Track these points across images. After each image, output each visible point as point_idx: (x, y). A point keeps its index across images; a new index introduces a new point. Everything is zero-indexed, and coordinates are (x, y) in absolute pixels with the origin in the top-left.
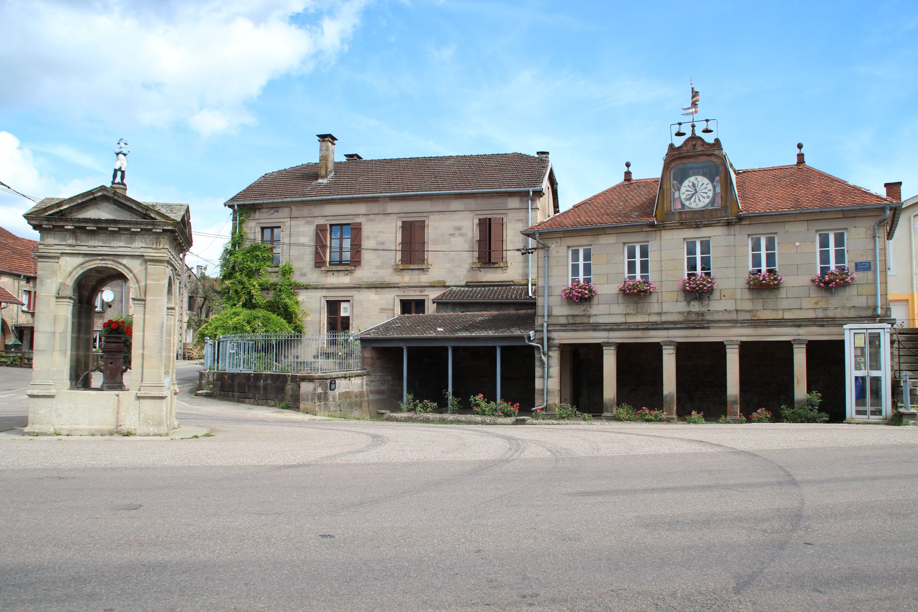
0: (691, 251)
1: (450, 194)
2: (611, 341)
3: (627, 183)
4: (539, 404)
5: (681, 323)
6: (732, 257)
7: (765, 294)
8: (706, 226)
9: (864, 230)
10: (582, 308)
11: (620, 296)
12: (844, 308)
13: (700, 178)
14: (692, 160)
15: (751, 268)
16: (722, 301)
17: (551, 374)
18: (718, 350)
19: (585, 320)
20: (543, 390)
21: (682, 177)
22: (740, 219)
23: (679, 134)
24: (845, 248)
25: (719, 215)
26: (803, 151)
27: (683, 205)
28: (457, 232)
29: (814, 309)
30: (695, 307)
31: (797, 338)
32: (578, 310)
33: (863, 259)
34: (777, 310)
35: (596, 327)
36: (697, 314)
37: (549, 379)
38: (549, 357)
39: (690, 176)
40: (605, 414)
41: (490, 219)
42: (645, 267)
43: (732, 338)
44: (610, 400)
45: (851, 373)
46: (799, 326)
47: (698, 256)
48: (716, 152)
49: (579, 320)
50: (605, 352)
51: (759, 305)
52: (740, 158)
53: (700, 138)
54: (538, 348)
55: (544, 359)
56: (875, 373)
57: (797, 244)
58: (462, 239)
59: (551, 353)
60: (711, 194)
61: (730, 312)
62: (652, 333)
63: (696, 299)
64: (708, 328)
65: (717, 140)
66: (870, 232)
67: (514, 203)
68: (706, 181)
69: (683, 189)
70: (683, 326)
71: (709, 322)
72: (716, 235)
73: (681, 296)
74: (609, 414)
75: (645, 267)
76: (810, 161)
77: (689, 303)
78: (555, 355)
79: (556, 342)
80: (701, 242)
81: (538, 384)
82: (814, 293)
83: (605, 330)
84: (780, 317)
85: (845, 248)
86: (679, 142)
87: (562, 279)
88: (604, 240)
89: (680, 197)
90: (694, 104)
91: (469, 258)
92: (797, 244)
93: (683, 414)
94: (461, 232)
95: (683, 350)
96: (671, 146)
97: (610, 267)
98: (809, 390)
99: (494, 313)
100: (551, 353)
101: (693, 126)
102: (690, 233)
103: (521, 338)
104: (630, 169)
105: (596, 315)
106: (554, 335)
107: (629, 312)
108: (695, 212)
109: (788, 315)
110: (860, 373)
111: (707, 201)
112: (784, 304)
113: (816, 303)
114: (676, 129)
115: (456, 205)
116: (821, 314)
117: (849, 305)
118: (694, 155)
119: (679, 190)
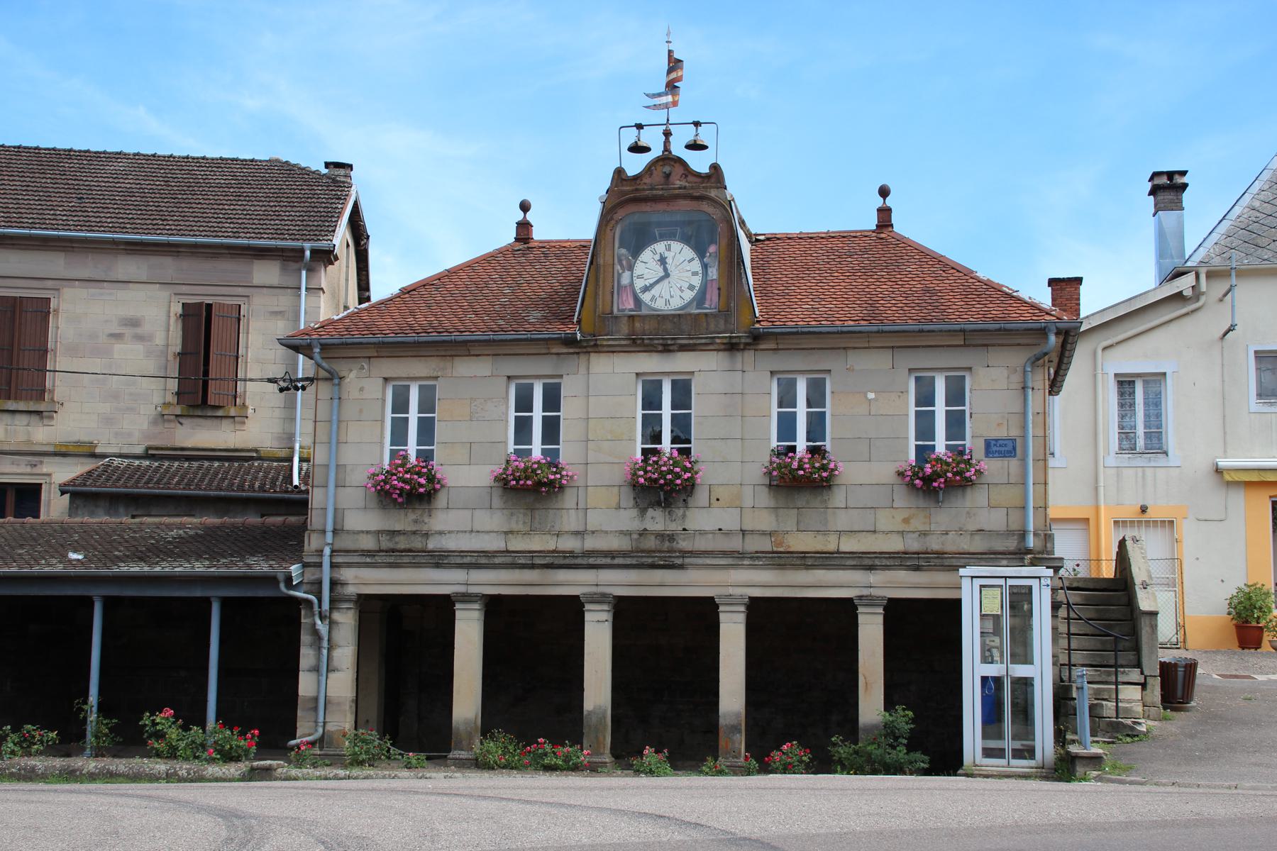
1: (222, 246)
2: (473, 590)
3: (520, 246)
4: (306, 730)
5: (624, 554)
6: (737, 417)
7: (802, 499)
8: (684, 348)
9: (1005, 373)
11: (497, 493)
12: (961, 531)
13: (676, 246)
14: (661, 206)
15: (774, 443)
18: (703, 614)
19: (417, 543)
20: (316, 699)
21: (639, 241)
23: (637, 149)
25: (712, 327)
28: (128, 331)
29: (902, 533)
30: (657, 521)
31: (865, 592)
32: (402, 521)
33: (1001, 433)
34: (826, 532)
35: (440, 560)
36: (660, 536)
37: (331, 677)
40: (455, 754)
41: (209, 306)
42: (551, 430)
43: (731, 591)
46: (871, 568)
48: (713, 193)
49: (402, 543)
51: (789, 520)
52: (766, 204)
53: (680, 161)
54: (309, 602)
56: (1021, 671)
57: (871, 396)
58: (139, 347)
59: (337, 616)
60: (697, 281)
62: (562, 575)
63: (659, 504)
65: (715, 168)
66: (1016, 378)
67: (266, 272)
68: (688, 252)
69: (639, 268)
70: (628, 561)
71: (685, 554)
72: (706, 370)
73: (627, 497)
74: (464, 755)
75: (551, 430)
77: (643, 511)
78: (347, 620)
79: (351, 590)
80: (674, 383)
81: (306, 685)
82: (902, 499)
84: (832, 547)
86: (635, 165)
87: (369, 449)
89: (632, 284)
91: (158, 392)
92: (871, 396)
93: (626, 754)
94: (139, 331)
95: (628, 613)
96: (619, 172)
97: (476, 427)
98: (889, 705)
100: (337, 616)
101: (667, 134)
102: (651, 363)
103: (271, 580)
105: (441, 533)
106: (347, 574)
107: (515, 527)
108: (662, 318)
109: (848, 545)
110: (992, 670)
111: (689, 295)
112: (842, 521)
113: (906, 521)
114: (630, 137)
115: (128, 267)
116: (914, 545)
117: (972, 527)
118: (666, 195)
119: (631, 268)
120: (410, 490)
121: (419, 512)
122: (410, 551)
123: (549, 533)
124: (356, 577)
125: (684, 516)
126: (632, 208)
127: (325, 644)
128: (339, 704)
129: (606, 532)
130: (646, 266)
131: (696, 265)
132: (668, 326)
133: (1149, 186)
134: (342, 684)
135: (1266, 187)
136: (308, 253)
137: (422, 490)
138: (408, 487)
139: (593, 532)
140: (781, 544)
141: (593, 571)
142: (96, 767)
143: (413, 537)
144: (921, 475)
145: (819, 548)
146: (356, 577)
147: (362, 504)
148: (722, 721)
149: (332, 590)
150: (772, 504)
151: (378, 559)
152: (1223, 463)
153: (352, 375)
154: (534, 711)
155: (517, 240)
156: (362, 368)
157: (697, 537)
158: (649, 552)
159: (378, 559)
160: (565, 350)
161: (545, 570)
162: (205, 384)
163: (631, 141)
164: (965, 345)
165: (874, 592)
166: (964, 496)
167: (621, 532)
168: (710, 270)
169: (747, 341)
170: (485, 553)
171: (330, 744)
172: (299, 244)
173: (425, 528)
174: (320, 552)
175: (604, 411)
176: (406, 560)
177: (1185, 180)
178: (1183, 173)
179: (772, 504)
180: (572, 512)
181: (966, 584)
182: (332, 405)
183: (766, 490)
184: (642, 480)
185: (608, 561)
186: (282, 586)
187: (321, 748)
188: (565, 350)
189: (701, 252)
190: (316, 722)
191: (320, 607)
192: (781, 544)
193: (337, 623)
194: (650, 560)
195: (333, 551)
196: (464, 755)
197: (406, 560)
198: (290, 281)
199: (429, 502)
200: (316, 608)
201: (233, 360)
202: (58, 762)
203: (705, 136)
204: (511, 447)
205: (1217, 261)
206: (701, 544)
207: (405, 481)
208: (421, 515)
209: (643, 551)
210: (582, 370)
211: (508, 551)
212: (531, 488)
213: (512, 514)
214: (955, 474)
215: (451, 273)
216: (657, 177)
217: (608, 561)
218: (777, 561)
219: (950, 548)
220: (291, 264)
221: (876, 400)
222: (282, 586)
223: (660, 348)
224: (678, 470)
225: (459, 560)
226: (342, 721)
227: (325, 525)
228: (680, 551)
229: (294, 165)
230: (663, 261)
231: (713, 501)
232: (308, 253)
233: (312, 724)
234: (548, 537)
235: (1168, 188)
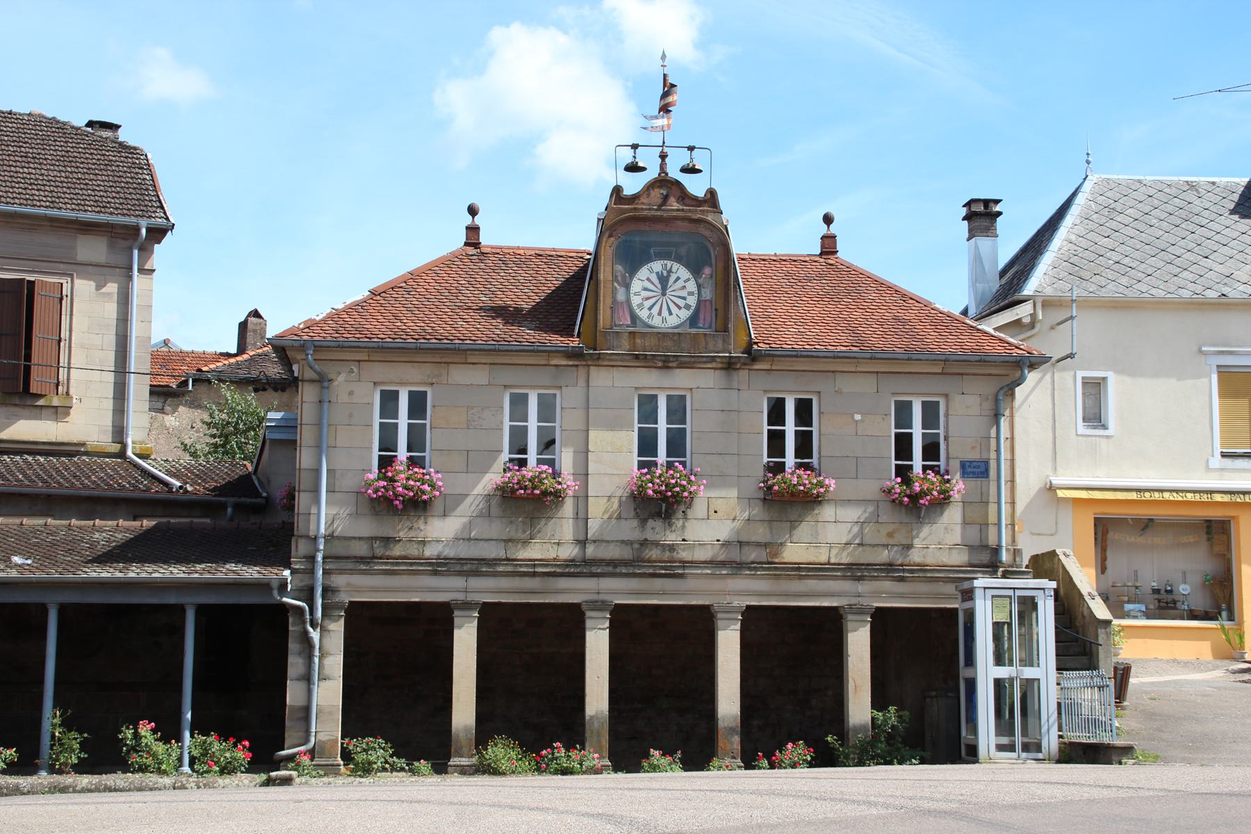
2: (472, 597)
3: (471, 251)
5: (626, 563)
8: (683, 365)
9: (978, 400)
14: (659, 227)
15: (766, 459)
16: (713, 522)
17: (327, 671)
18: (700, 623)
19: (413, 551)
21: (633, 259)
22: (752, 355)
23: (633, 168)
24: (428, 422)
25: (711, 346)
26: (834, 229)
27: (634, 318)
29: (886, 546)
31: (854, 601)
38: (323, 630)
39: (650, 260)
40: (454, 761)
44: (467, 729)
45: (987, 672)
47: (662, 426)
48: (710, 218)
53: (678, 183)
55: (315, 635)
56: (1029, 673)
57: (858, 417)
60: (692, 301)
62: (563, 583)
64: (681, 576)
65: (712, 194)
66: (988, 405)
67: (92, 249)
69: (636, 285)
71: (685, 564)
72: (698, 385)
74: (464, 761)
77: (643, 522)
78: (337, 628)
79: (345, 598)
80: (669, 398)
81: (294, 694)
83: (460, 573)
85: (428, 422)
86: (633, 184)
88: (461, 375)
89: (628, 301)
90: (665, 109)
92: (858, 417)
93: (627, 756)
95: (625, 623)
96: (617, 190)
98: (879, 702)
99: (147, 523)
101: (663, 156)
102: (648, 379)
104: (478, 220)
106: (339, 581)
107: (513, 535)
108: (663, 336)
110: (1003, 672)
111: (685, 314)
113: (890, 535)
114: (627, 156)
118: (662, 218)
119: (627, 287)
125: (683, 527)
127: (317, 653)
128: (330, 713)
129: (608, 542)
130: (644, 280)
133: (964, 211)
135: (1078, 222)
137: (425, 497)
139: (595, 541)
141: (595, 579)
142: (90, 783)
148: (721, 724)
152: (1056, 481)
153: (341, 378)
154: (533, 716)
155: (466, 244)
156: (352, 371)
157: (697, 549)
160: (564, 362)
161: (546, 578)
162: (28, 370)
163: (629, 160)
164: (942, 374)
166: (942, 513)
167: (623, 542)
168: (703, 291)
170: (482, 561)
172: (133, 220)
177: (998, 208)
178: (997, 202)
181: (978, 594)
184: (650, 492)
186: (275, 593)
188: (564, 362)
189: (696, 271)
196: (464, 761)
198: (120, 259)
201: (55, 343)
202: (95, 779)
203: (700, 160)
205: (1049, 291)
207: (406, 488)
214: (939, 493)
215: (414, 276)
216: (657, 194)
217: (610, 569)
220: (120, 241)
221: (862, 421)
222: (275, 593)
224: (684, 483)
225: (458, 568)
229: (64, 124)
232: (144, 231)
233: (301, 734)
235: (982, 216)
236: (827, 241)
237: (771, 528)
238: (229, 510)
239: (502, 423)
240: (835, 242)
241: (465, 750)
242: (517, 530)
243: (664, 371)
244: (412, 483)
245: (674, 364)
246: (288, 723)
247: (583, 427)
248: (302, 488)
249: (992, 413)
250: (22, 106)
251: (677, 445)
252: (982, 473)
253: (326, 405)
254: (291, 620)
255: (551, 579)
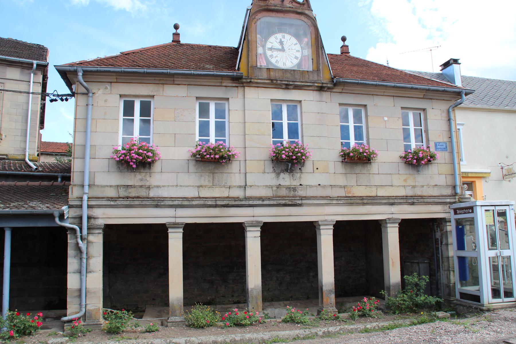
0: (277, 114)
2: (179, 220)
4: (73, 310)
5: (269, 199)
6: (322, 125)
7: (358, 169)
10: (139, 176)
11: (192, 164)
12: (428, 186)
13: (287, 36)
17: (91, 267)
19: (143, 193)
20: (80, 290)
29: (404, 186)
30: (286, 180)
31: (390, 216)
32: (133, 179)
34: (370, 186)
35: (158, 203)
36: (289, 188)
37: (86, 276)
40: (172, 319)
42: (220, 128)
43: (326, 218)
46: (392, 204)
48: (307, 12)
49: (133, 193)
50: (170, 235)
51: (352, 180)
54: (73, 230)
57: (386, 119)
59: (91, 238)
60: (299, 55)
61: (324, 187)
63: (287, 170)
64: (300, 205)
66: (445, 115)
68: (294, 40)
70: (272, 202)
71: (302, 198)
72: (308, 99)
73: (269, 167)
74: (178, 319)
75: (220, 128)
76: (353, 53)
77: (278, 174)
78: (97, 241)
79: (101, 222)
82: (403, 169)
83: (171, 206)
84: (373, 194)
87: (115, 133)
92: (386, 119)
97: (177, 124)
100: (91, 238)
103: (50, 216)
105: (158, 187)
106: (97, 212)
107: (203, 183)
109: (381, 193)
111: (295, 62)
112: (377, 180)
113: (405, 180)
116: (410, 193)
117: (433, 184)
120: (136, 161)
121: (143, 174)
122: (138, 197)
123: (224, 186)
124: (104, 214)
125: (300, 177)
126: (265, 14)
127: (84, 256)
128: (95, 292)
131: (298, 47)
132: (288, 75)
134: (95, 280)
136: (35, 66)
137: (149, 160)
138: (141, 158)
139: (251, 186)
140: (350, 192)
143: (140, 189)
144: (415, 157)
145: (368, 194)
146: (104, 214)
147: (107, 169)
148: (324, 288)
149: (88, 221)
150: (344, 172)
151: (119, 203)
153: (100, 92)
155: (173, 41)
156: (106, 88)
157: (308, 189)
158: (283, 197)
159: (119, 203)
160: (230, 85)
161: (223, 209)
165: (395, 216)
166: (428, 169)
168: (304, 51)
169: (332, 85)
171: (90, 317)
173: (148, 184)
174: (81, 199)
175: (249, 120)
176: (137, 203)
179: (344, 172)
180: (237, 175)
181: (478, 209)
182: (87, 109)
183: (340, 164)
184: (284, 156)
185: (260, 202)
186: (57, 220)
187: (85, 320)
188: (230, 85)
189: (300, 41)
190: (80, 304)
191: (81, 233)
192: (350, 192)
193: (92, 242)
194: (284, 202)
195: (88, 198)
197: (137, 203)
199: (150, 168)
200: (79, 234)
204: (197, 138)
206: (310, 193)
207: (139, 154)
208: (145, 176)
209: (279, 197)
210: (240, 95)
211: (200, 198)
212: (212, 159)
213: (201, 176)
218: (349, 201)
219: (425, 194)
221: (388, 121)
222: (57, 220)
223: (284, 87)
225: (170, 203)
226: (96, 303)
227: (83, 181)
228: (300, 197)
230: (281, 43)
231: (315, 169)
232: (35, 66)
233: (77, 306)
234: (223, 189)
236: (344, 48)
237: (346, 178)
238: (59, 179)
239: (195, 118)
240: (348, 48)
241: (178, 312)
242: (205, 180)
243: (286, 91)
244: (141, 151)
245: (292, 87)
246: (68, 300)
247: (242, 121)
248: (76, 156)
249: (447, 119)
250: (5, 36)
251: (293, 131)
252: (445, 149)
253: (90, 107)
254: (69, 236)
255: (225, 208)
